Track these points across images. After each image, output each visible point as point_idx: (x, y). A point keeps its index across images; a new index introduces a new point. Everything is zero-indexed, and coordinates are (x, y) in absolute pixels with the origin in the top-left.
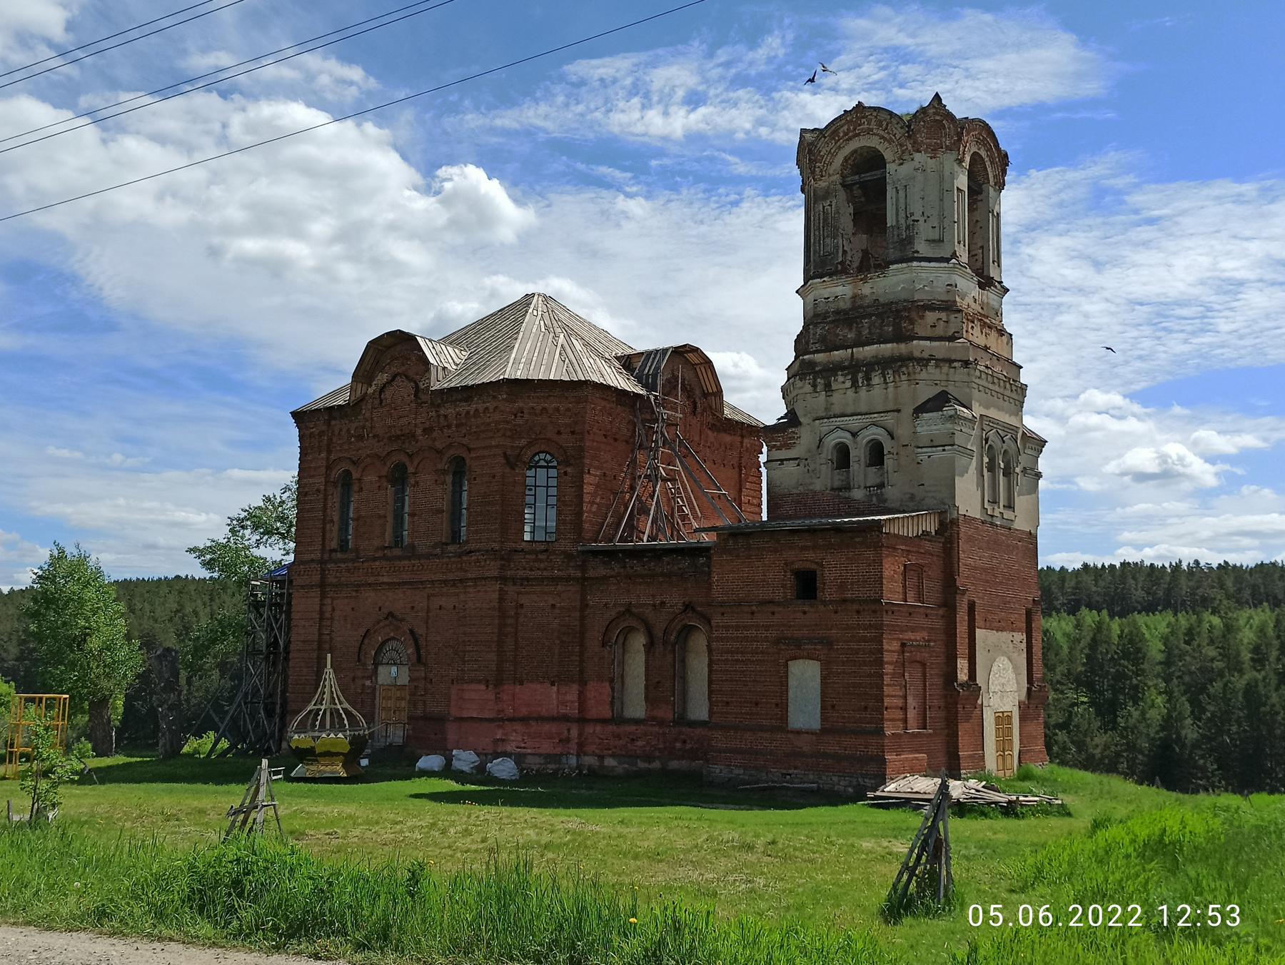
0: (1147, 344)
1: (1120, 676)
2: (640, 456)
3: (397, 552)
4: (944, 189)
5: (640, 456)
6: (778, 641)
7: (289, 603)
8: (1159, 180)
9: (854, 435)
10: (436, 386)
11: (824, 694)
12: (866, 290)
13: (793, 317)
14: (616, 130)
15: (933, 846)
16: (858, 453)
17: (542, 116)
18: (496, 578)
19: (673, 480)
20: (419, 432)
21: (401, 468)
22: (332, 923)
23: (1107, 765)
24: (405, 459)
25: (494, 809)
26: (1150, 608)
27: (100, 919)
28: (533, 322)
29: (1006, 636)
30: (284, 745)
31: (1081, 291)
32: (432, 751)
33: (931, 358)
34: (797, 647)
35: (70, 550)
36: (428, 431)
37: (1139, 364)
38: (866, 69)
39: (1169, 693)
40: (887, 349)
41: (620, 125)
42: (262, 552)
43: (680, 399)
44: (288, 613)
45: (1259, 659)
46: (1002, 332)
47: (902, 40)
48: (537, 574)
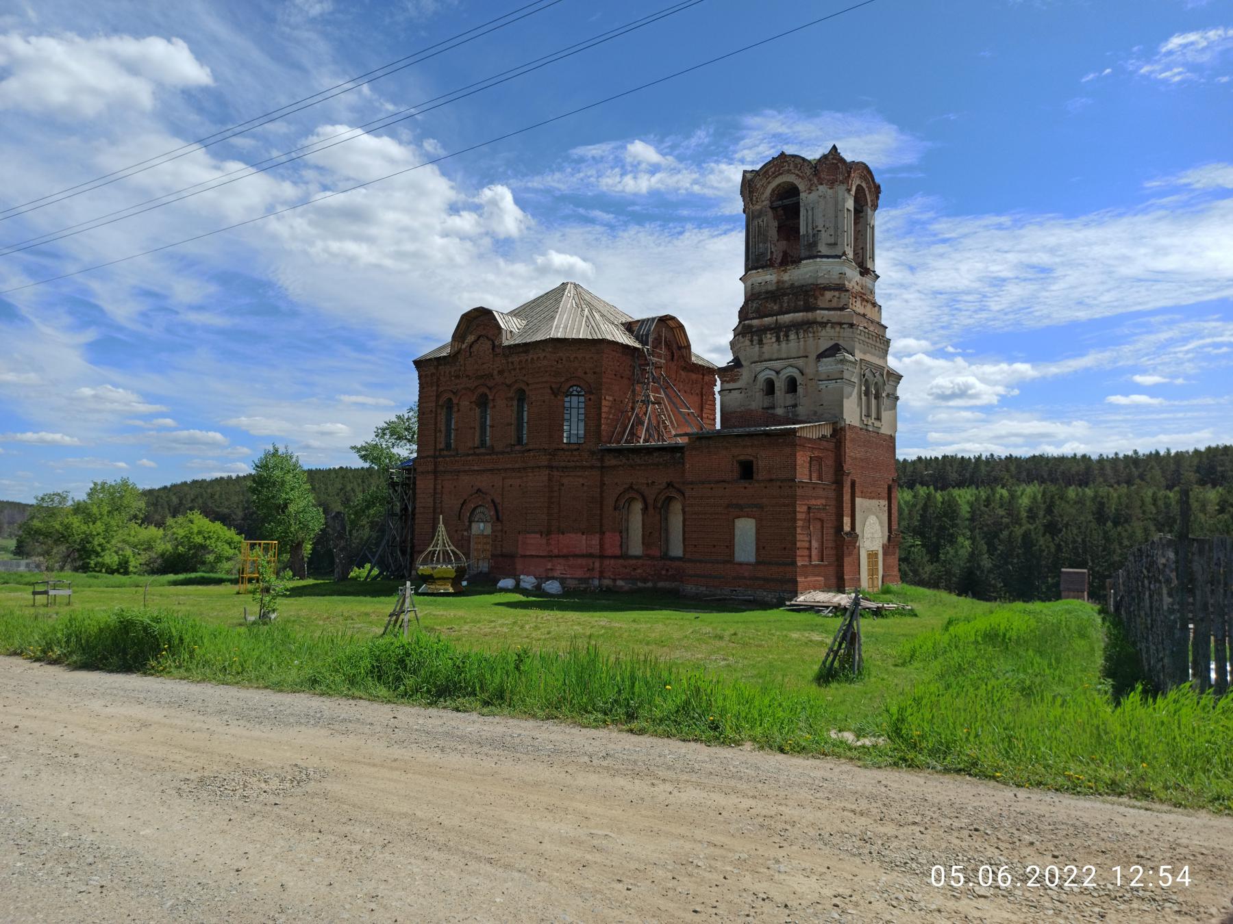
0: (945, 319)
1: (942, 528)
2: (638, 388)
3: (483, 450)
4: (838, 209)
5: (638, 388)
6: (728, 506)
7: (414, 484)
8: (948, 216)
9: (778, 373)
10: (506, 343)
11: (758, 539)
12: (786, 277)
13: (736, 294)
14: (605, 189)
15: (850, 637)
16: (780, 385)
17: (558, 181)
18: (547, 467)
19: (659, 403)
20: (495, 372)
21: (484, 396)
22: (466, 688)
23: (933, 584)
24: (487, 391)
25: (552, 613)
26: (960, 484)
27: (313, 684)
28: (568, 301)
29: (875, 502)
30: (413, 572)
31: (902, 286)
32: (507, 576)
33: (829, 322)
34: (741, 510)
35: (281, 450)
36: (500, 373)
37: (942, 332)
38: (761, 148)
39: (973, 539)
40: (799, 316)
41: (607, 185)
42: (395, 450)
43: (663, 351)
44: (414, 490)
45: (1032, 516)
46: (874, 304)
47: (784, 130)
48: (572, 464)
